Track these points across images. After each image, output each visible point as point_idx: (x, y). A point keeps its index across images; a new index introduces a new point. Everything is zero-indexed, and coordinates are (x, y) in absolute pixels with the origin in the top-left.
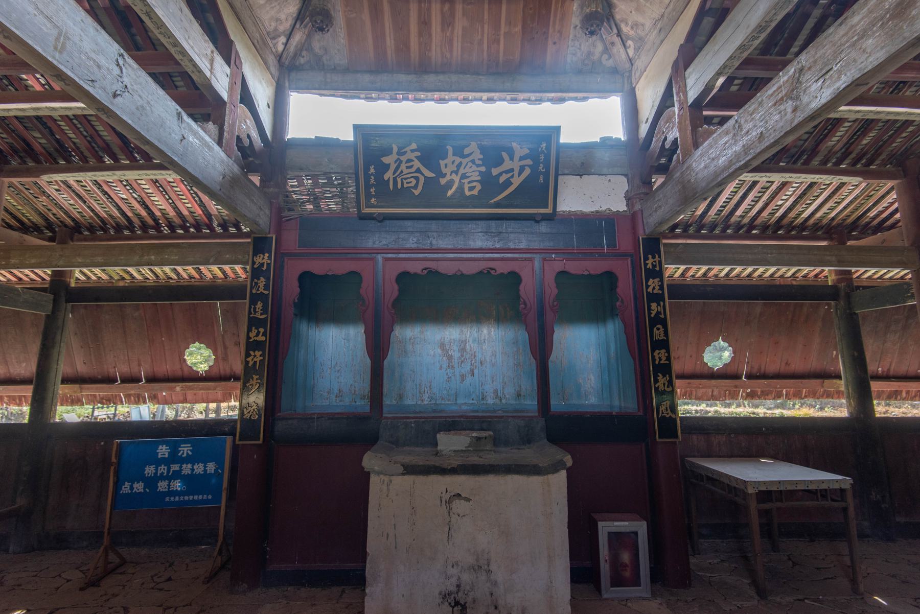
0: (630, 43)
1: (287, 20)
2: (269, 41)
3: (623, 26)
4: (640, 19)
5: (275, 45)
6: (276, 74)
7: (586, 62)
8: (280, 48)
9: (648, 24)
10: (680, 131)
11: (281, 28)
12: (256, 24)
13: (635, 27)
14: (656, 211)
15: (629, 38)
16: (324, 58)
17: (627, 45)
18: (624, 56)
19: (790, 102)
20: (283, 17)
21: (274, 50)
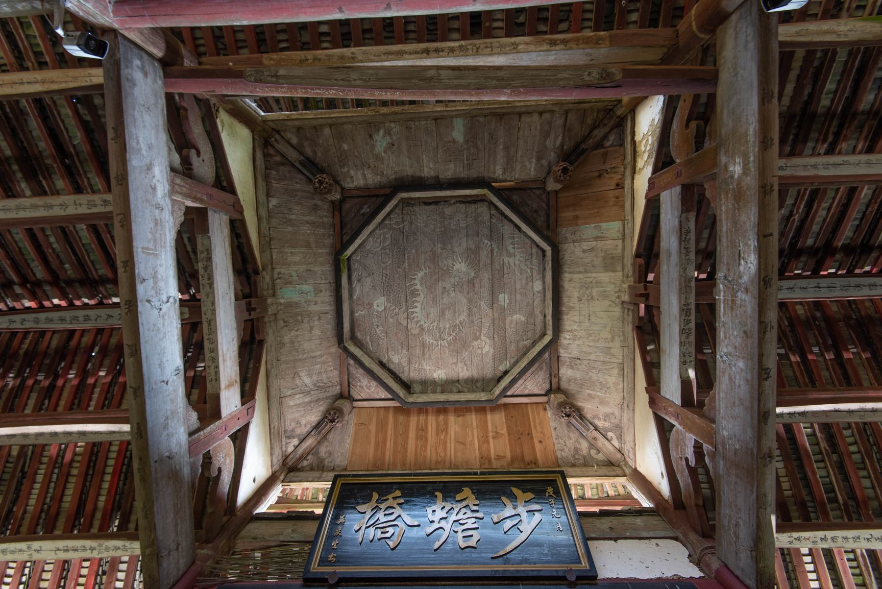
0: (610, 434)
1: (306, 425)
2: (283, 439)
3: (596, 422)
4: (608, 410)
5: (287, 444)
6: (276, 467)
7: (577, 457)
8: (290, 449)
9: (617, 412)
10: (690, 430)
11: (298, 431)
12: (279, 418)
13: (607, 419)
14: (737, 537)
15: (608, 430)
16: (326, 461)
17: (609, 437)
18: (611, 448)
19: (739, 294)
20: (303, 422)
21: (284, 449)
